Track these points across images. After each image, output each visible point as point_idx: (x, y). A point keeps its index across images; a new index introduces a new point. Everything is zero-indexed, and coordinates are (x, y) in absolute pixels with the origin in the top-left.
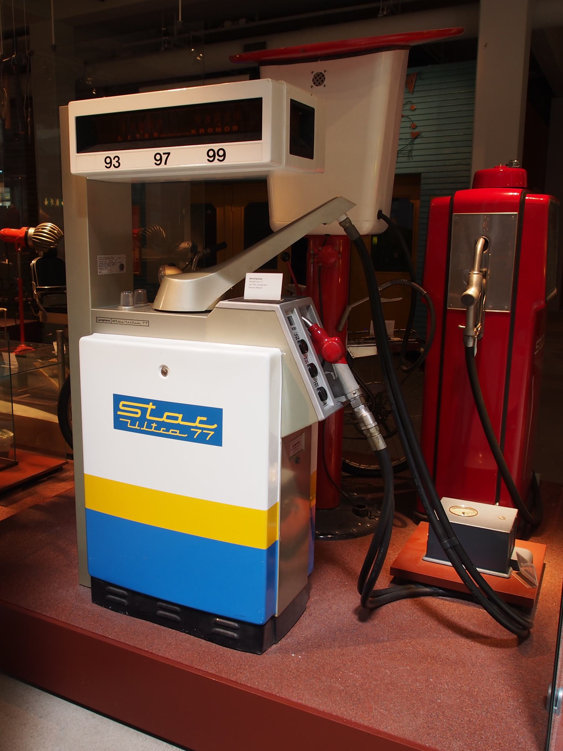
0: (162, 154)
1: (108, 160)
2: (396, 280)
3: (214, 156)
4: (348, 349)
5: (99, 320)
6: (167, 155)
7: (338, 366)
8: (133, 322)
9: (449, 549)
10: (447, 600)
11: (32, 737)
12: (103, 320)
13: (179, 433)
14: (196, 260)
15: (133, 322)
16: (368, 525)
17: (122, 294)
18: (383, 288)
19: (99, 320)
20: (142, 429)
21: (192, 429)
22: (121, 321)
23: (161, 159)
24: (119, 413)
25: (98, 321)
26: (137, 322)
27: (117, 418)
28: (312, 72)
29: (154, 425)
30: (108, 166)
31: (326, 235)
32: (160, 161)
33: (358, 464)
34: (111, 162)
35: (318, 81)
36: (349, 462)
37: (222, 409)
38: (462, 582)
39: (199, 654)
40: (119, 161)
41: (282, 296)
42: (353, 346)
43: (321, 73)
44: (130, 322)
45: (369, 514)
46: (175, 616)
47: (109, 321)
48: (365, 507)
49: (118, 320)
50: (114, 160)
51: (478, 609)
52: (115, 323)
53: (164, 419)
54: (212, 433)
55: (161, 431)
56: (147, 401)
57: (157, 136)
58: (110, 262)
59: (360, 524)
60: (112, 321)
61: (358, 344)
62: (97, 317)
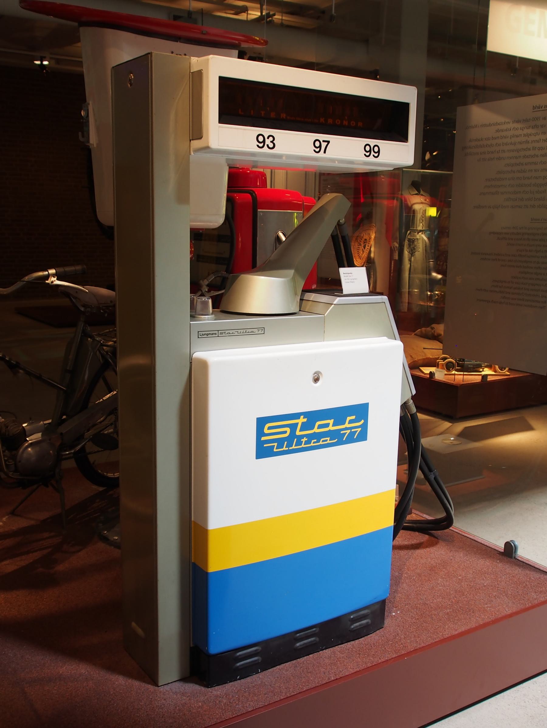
0: (322, 142)
1: (261, 139)
3: (370, 151)
5: (202, 334)
6: (327, 143)
8: (246, 331)
12: (208, 335)
13: (330, 440)
15: (246, 331)
19: (202, 334)
20: (290, 448)
21: (342, 432)
22: (231, 332)
23: (320, 147)
24: (263, 438)
25: (201, 337)
26: (250, 330)
27: (259, 444)
29: (305, 439)
30: (261, 145)
32: (319, 149)
34: (264, 142)
37: (257, 418)
39: (292, 675)
40: (274, 142)
44: (242, 332)
46: (312, 639)
47: (216, 334)
49: (227, 332)
50: (268, 139)
52: (224, 335)
53: (316, 430)
54: (359, 429)
55: (312, 444)
56: (296, 416)
57: (285, 118)
60: (219, 334)
62: (264, 328)
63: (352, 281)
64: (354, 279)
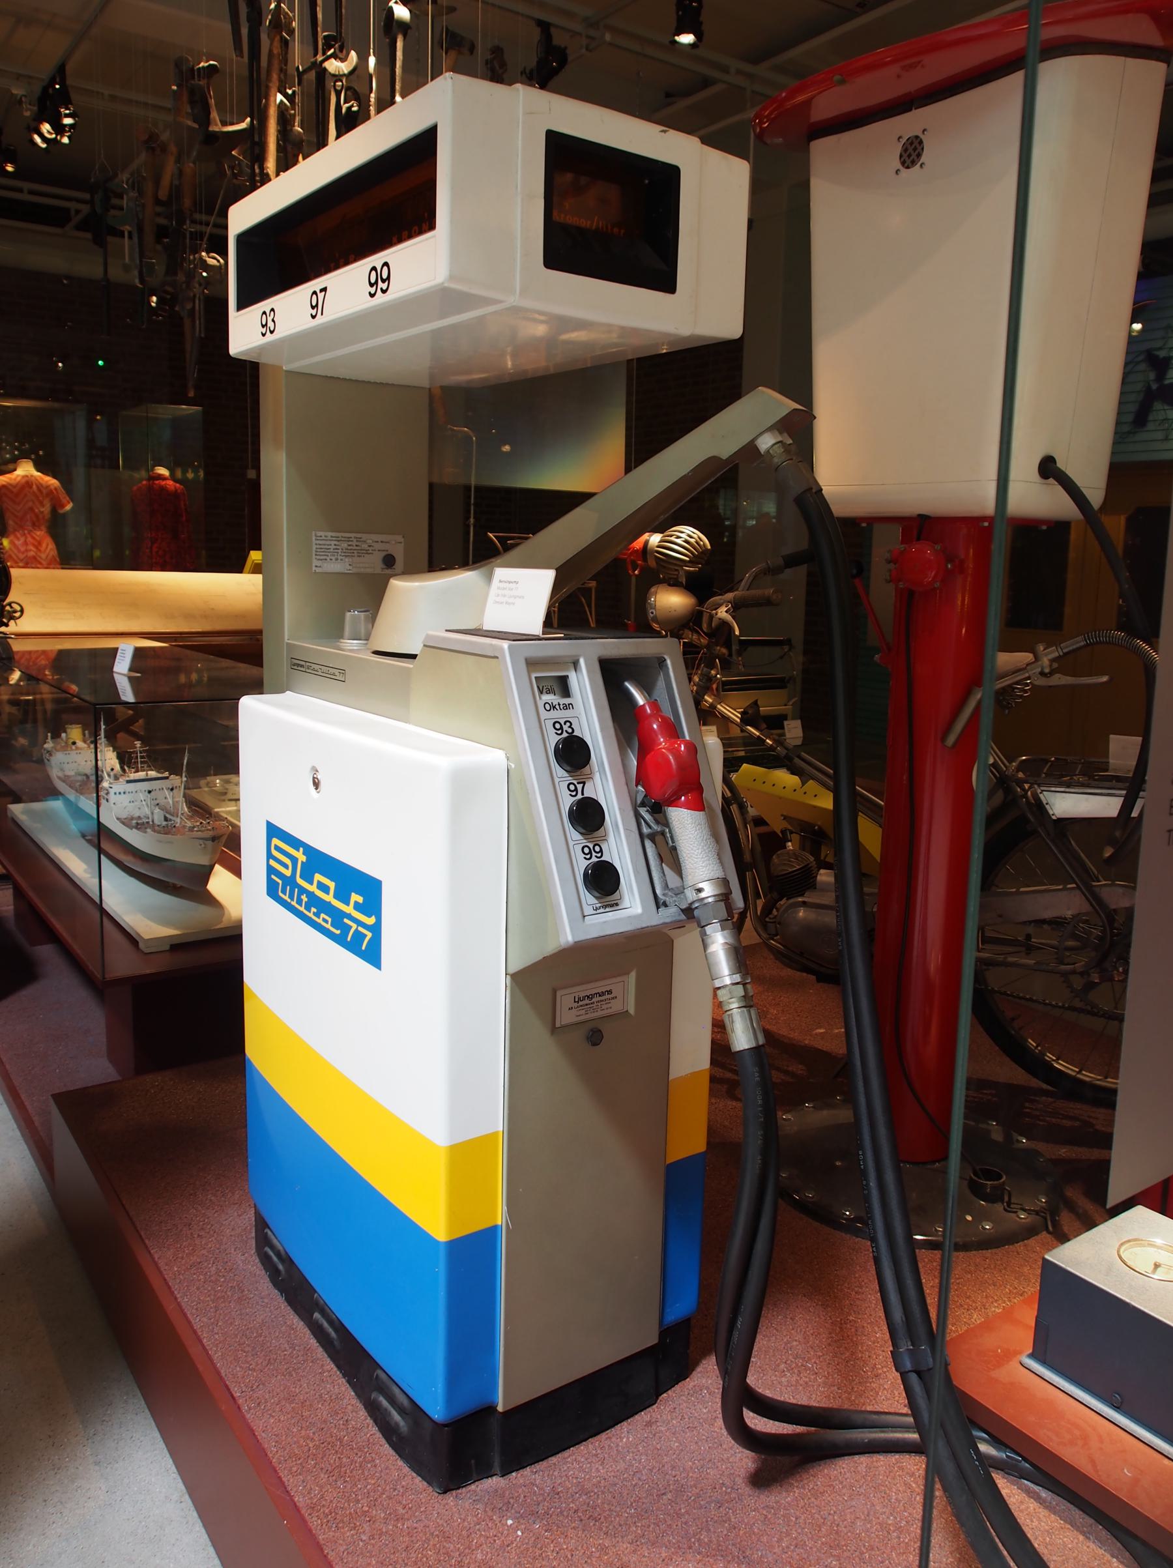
2: (1095, 632)
3: (590, 853)
4: (1041, 796)
7: (673, 814)
9: (910, 1374)
10: (1037, 1498)
11: (45, 1501)
14: (749, 577)
16: (987, 1227)
17: (348, 614)
18: (1065, 651)
21: (346, 920)
28: (900, 138)
31: (920, 516)
33: (1077, 1070)
34: (561, 728)
35: (909, 156)
36: (1053, 1060)
38: (995, 1478)
41: (548, 623)
42: (1053, 789)
43: (917, 137)
45: (1006, 1199)
48: (1000, 1177)
51: (1108, 1556)
58: (349, 548)
59: (969, 1218)
61: (1068, 787)
63: (511, 600)
64: (515, 597)
